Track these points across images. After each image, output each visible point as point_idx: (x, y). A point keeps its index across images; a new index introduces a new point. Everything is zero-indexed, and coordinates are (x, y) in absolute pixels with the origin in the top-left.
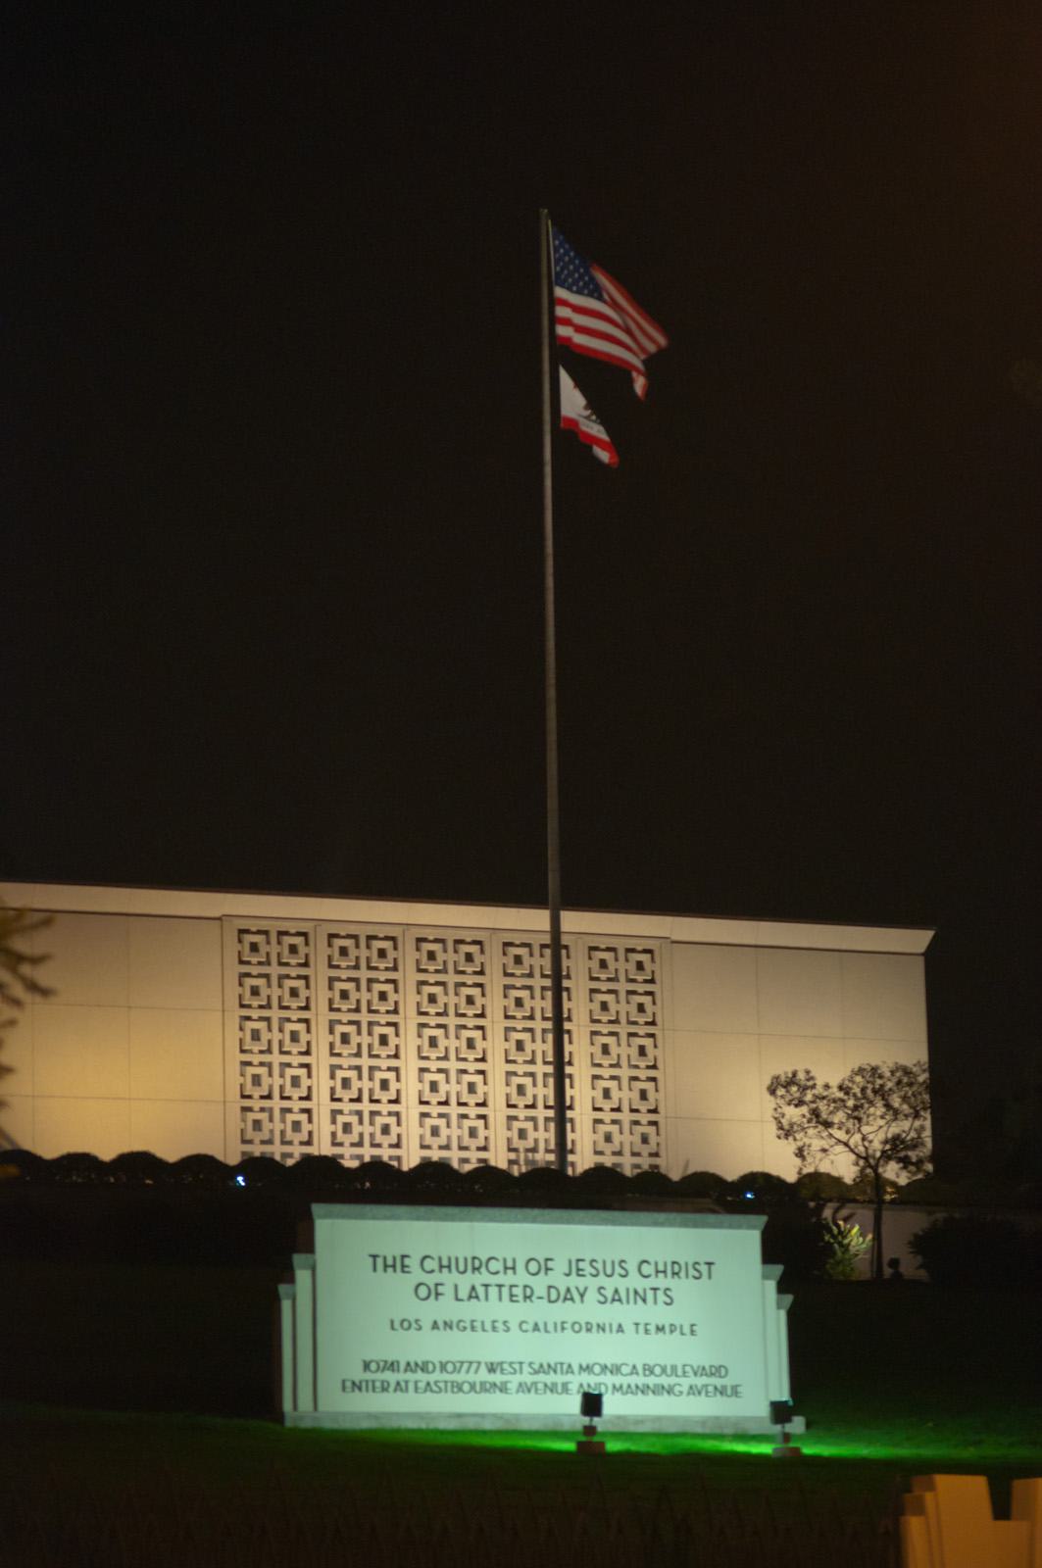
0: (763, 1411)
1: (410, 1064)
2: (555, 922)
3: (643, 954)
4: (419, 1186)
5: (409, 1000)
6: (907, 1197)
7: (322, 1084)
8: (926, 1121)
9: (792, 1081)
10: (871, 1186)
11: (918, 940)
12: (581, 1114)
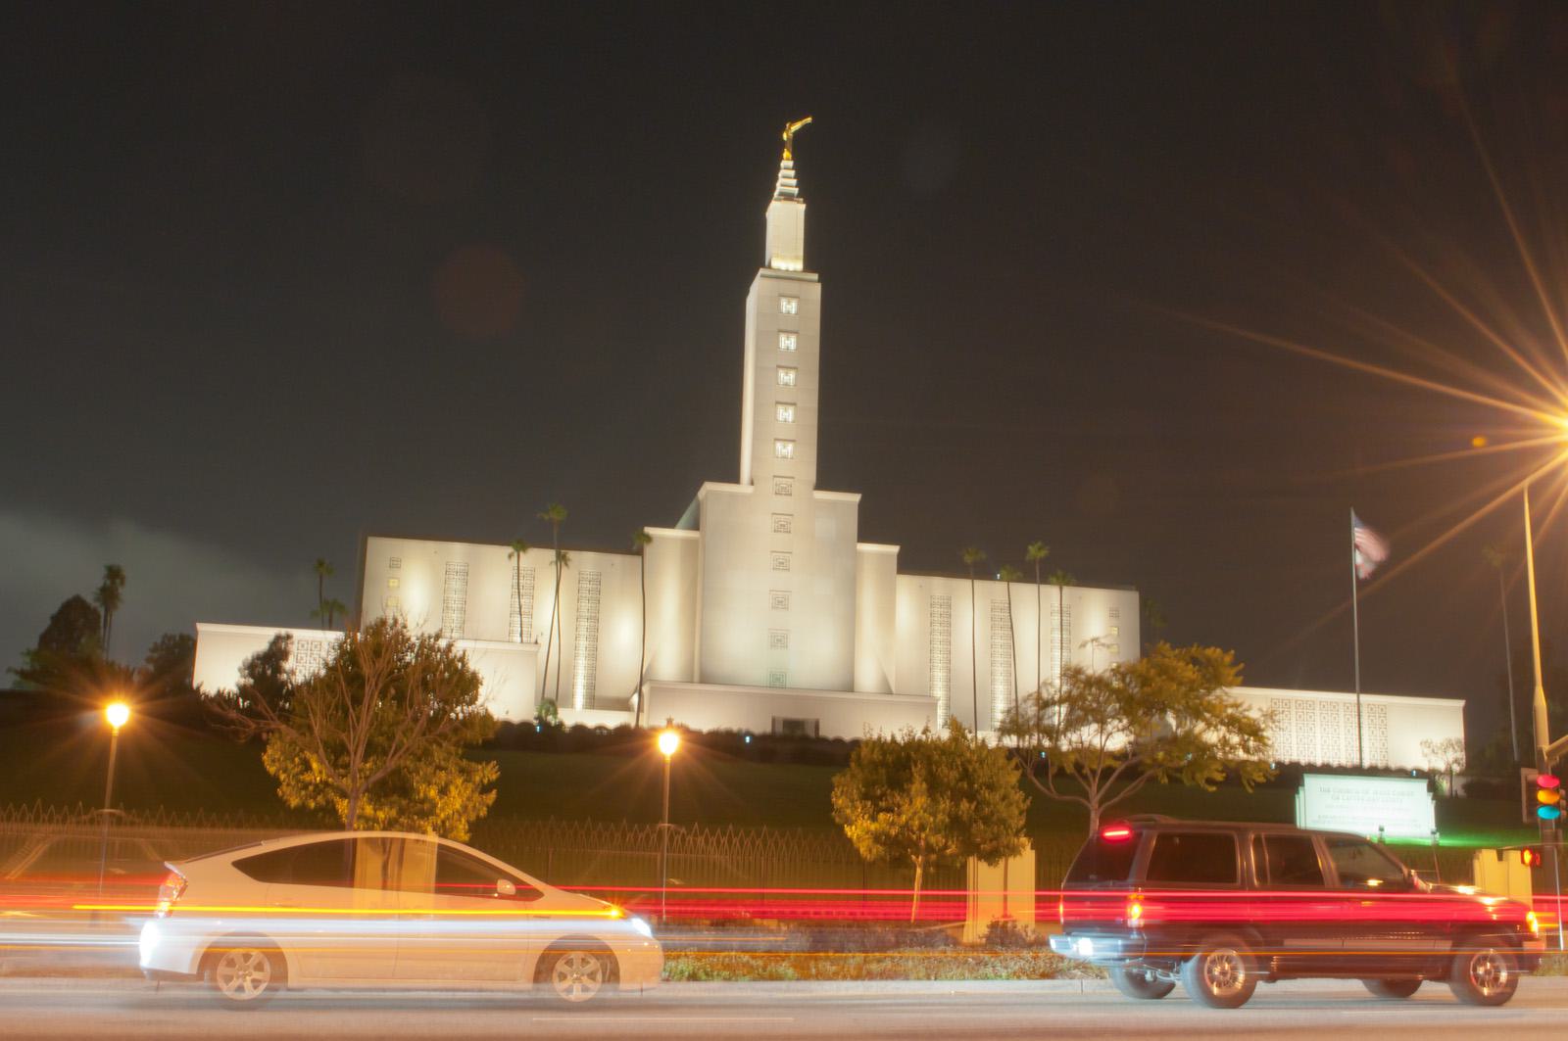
0: (1429, 833)
1: (1318, 735)
2: (1358, 698)
3: (1383, 709)
4: (1171, 719)
5: (1318, 718)
6: (1460, 774)
7: (1294, 740)
8: (1464, 753)
9: (1426, 742)
10: (1449, 772)
11: (856, 498)
12: (1366, 750)
